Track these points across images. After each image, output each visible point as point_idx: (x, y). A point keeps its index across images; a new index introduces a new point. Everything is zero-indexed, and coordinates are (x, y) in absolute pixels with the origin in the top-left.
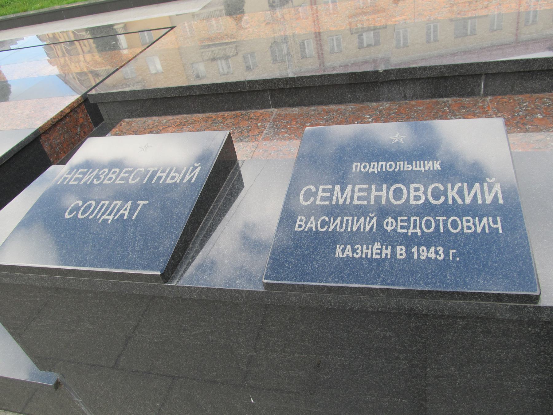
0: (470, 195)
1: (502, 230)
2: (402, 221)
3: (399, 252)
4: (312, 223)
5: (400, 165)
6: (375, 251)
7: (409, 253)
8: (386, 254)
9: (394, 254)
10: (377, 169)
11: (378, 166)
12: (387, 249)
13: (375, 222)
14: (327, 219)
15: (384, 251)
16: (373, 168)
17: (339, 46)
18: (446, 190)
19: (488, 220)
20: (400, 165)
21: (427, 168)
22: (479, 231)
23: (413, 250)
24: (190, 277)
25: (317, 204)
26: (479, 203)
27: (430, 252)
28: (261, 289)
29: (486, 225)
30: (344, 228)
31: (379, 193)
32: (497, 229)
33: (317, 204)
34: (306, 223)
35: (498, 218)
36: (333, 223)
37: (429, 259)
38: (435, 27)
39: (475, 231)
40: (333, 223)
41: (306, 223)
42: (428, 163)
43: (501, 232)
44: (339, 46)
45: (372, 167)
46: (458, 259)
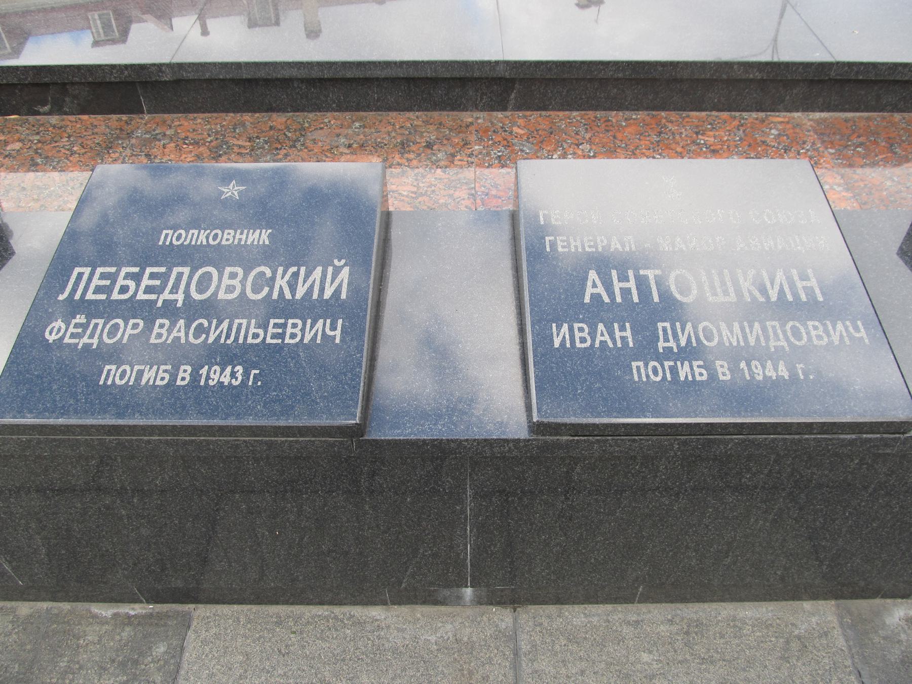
14: (206, 324)
18: (273, 279)
19: (324, 325)
26: (287, 297)
27: (780, 369)
28: (523, 434)
30: (232, 338)
32: (862, 338)
33: (138, 298)
35: (340, 322)
37: (221, 384)
39: (831, 343)
40: (222, 332)
41: (170, 331)
46: (259, 383)
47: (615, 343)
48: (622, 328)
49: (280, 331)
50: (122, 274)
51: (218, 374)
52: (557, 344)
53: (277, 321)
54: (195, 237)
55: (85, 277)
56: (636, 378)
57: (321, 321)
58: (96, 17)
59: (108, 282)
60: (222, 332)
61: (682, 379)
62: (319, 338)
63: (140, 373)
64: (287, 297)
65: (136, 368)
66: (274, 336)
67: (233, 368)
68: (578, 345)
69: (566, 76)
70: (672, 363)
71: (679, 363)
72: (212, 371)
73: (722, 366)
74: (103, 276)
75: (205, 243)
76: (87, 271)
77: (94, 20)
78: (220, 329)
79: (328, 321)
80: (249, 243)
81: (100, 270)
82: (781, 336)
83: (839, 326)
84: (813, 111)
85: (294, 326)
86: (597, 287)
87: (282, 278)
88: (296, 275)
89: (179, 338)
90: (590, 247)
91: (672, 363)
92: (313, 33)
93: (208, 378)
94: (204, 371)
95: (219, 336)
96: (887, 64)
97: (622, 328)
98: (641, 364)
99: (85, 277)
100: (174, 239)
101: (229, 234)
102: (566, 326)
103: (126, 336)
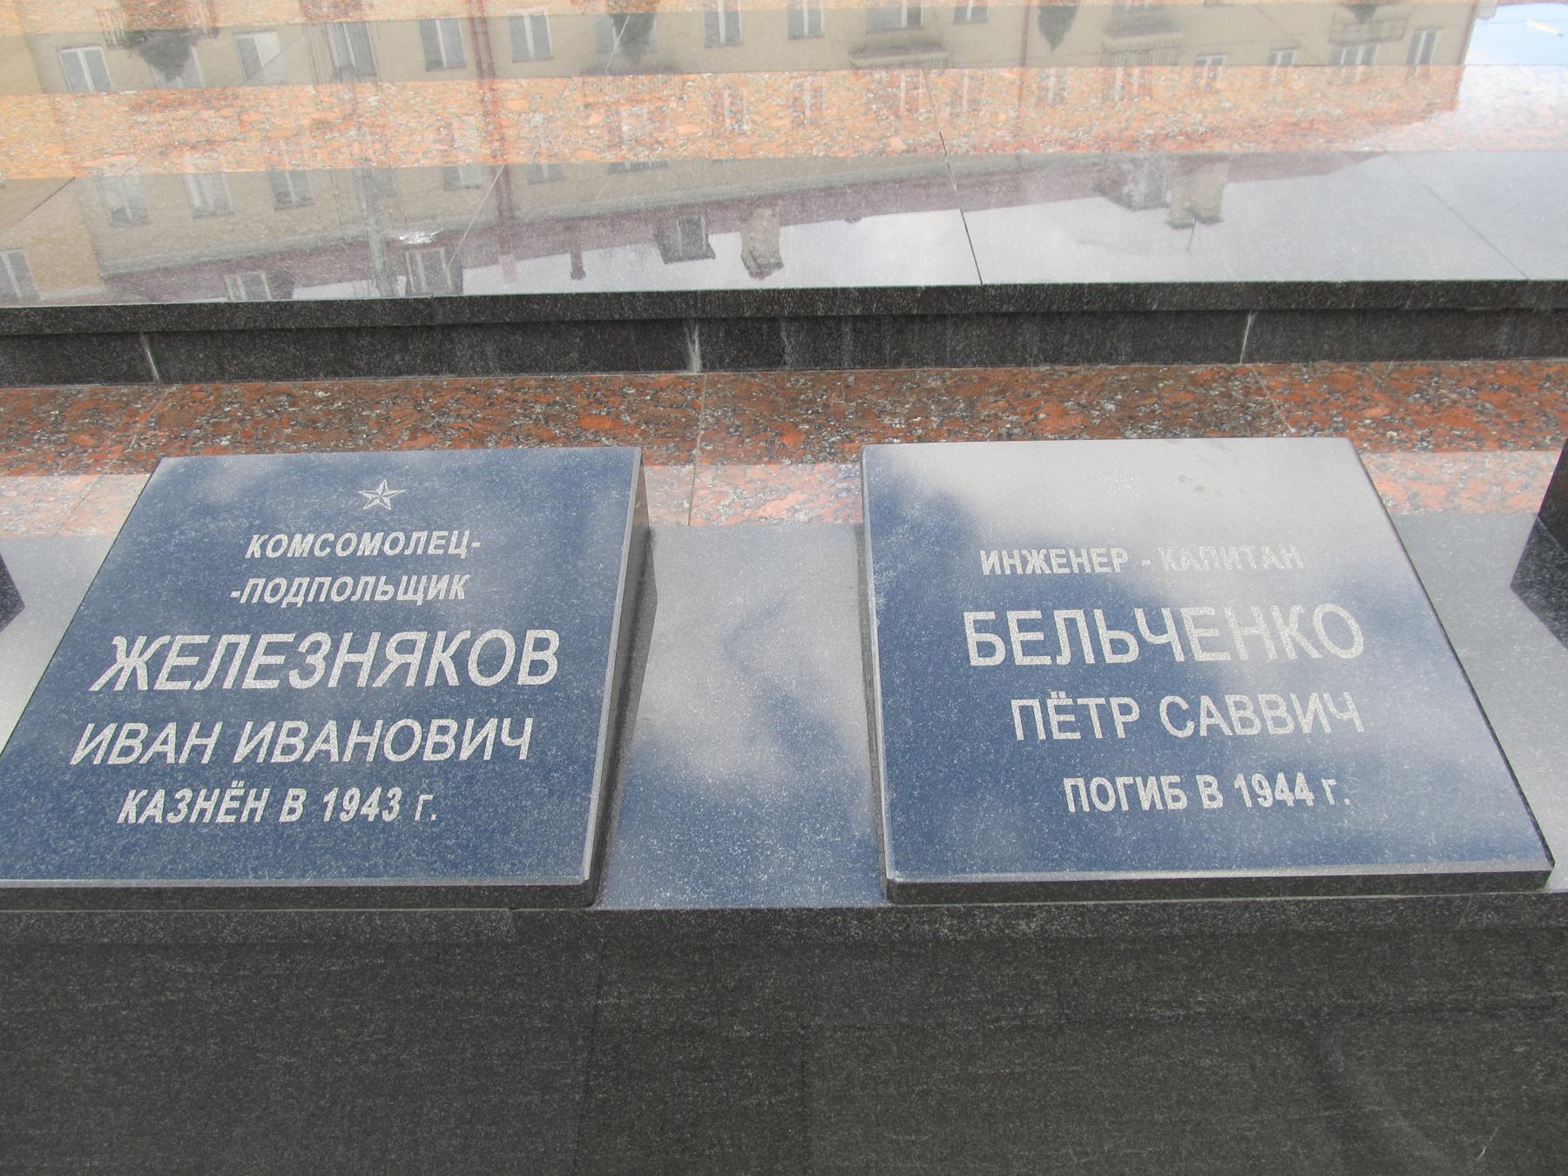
2: (1058, 556)
3: (289, 803)
4: (1210, 715)
5: (300, 585)
6: (216, 807)
8: (253, 811)
9: (1195, 798)
10: (306, 595)
11: (308, 590)
12: (258, 798)
13: (243, 741)
15: (250, 804)
16: (296, 594)
17: (817, 107)
20: (300, 585)
25: (244, 686)
26: (451, 683)
33: (244, 686)
37: (1279, 804)
38: (1431, 38)
40: (250, 739)
41: (309, 742)
44: (817, 107)
45: (294, 589)
50: (176, 648)
51: (357, 796)
54: (370, 588)
55: (241, 652)
56: (1072, 808)
57: (493, 722)
59: (193, 661)
60: (250, 739)
61: (1146, 806)
63: (171, 805)
64: (451, 683)
67: (385, 791)
70: (1129, 780)
71: (1139, 780)
72: (347, 798)
73: (1208, 785)
74: (272, 649)
75: (257, 555)
76: (244, 640)
79: (507, 722)
81: (266, 639)
83: (1314, 703)
87: (444, 649)
89: (163, 755)
91: (1129, 780)
92: (578, 272)
93: (338, 808)
94: (330, 798)
95: (256, 751)
99: (241, 652)
100: (268, 593)
103: (377, 731)
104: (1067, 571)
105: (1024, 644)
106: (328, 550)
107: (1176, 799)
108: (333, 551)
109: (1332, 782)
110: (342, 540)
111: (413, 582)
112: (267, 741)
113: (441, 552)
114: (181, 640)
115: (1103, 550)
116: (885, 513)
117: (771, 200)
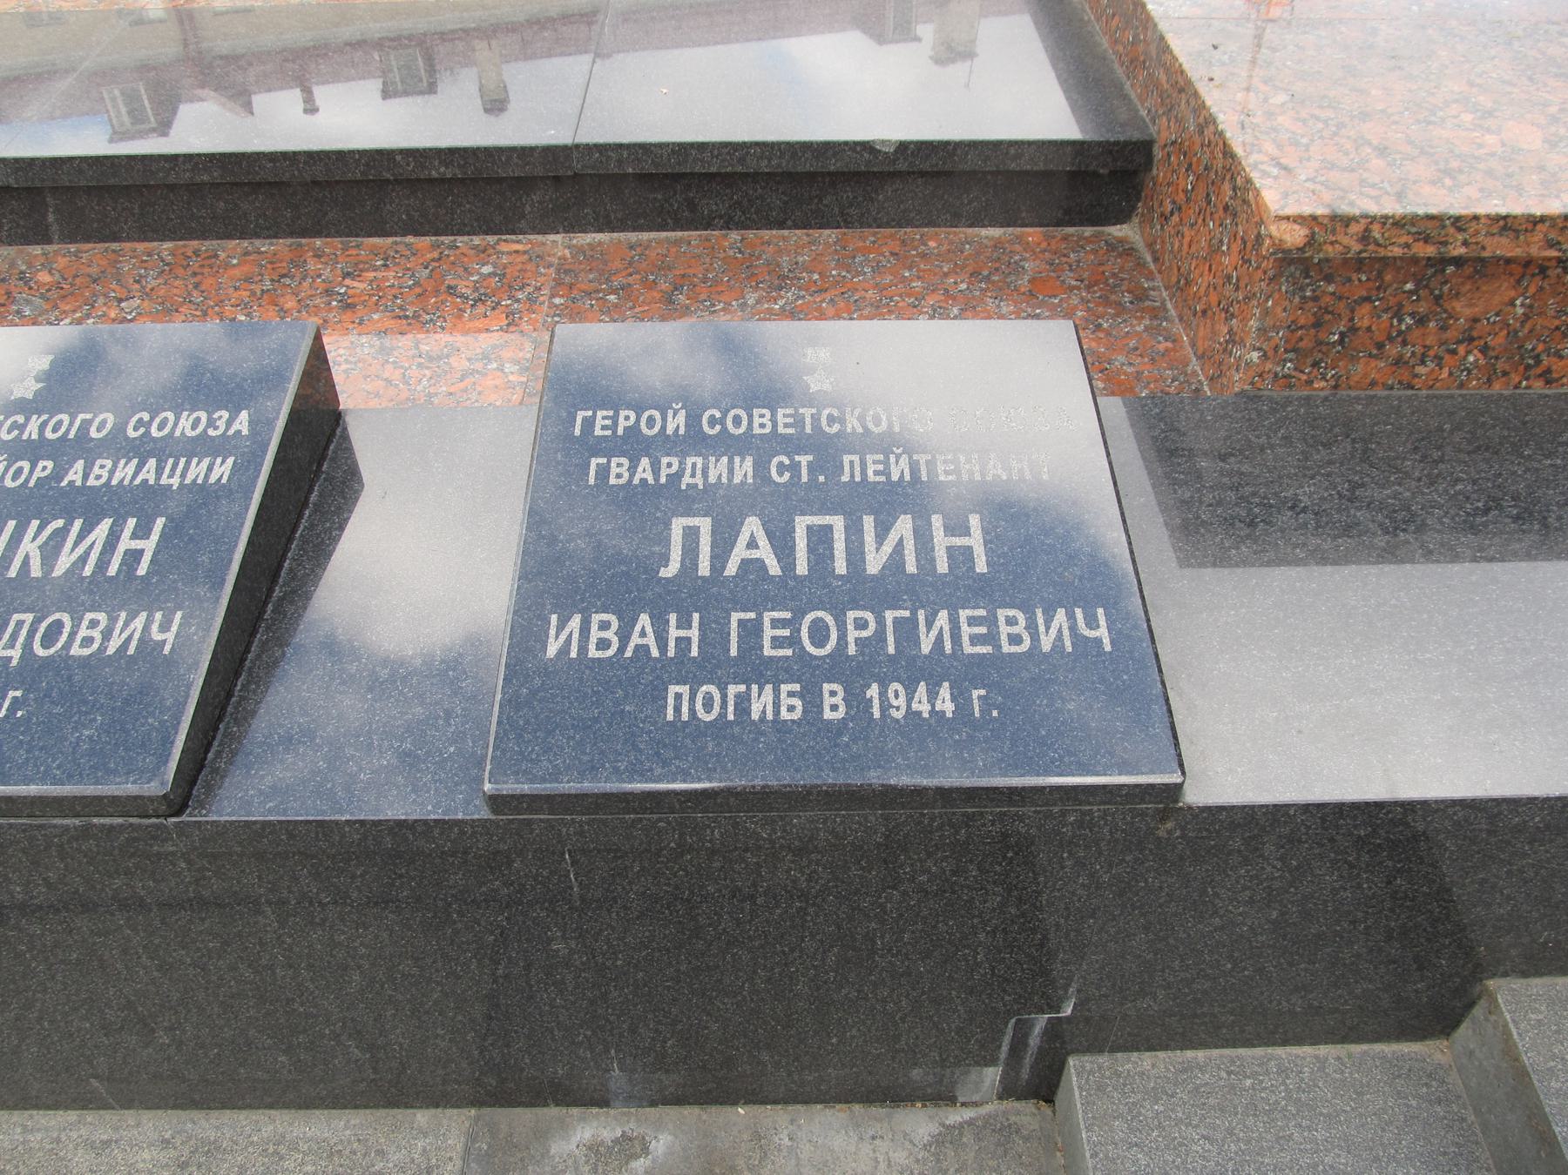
0: (748, 535)
1: (1112, 642)
2: (972, 621)
7: (856, 699)
16: (693, 475)
21: (712, 479)
22: (1046, 644)
23: (869, 694)
24: (254, 792)
26: (772, 572)
27: (916, 699)
28: (485, 813)
29: (1066, 633)
31: (683, 633)
32: (1098, 641)
34: (624, 638)
36: (87, 553)
40: (87, 553)
41: (624, 638)
42: (742, 461)
43: (1108, 648)
47: (663, 647)
48: (684, 623)
49: (786, 632)
52: (926, 648)
53: (776, 615)
56: (670, 716)
58: (117, 92)
61: (755, 716)
62: (134, 644)
64: (772, 572)
65: (733, 690)
66: (975, 640)
68: (593, 653)
69: (112, 181)
71: (755, 687)
73: (833, 693)
77: (113, 99)
78: (124, 636)
80: (212, 480)
82: (699, 472)
84: (584, 232)
85: (93, 624)
86: (757, 547)
87: (34, 539)
88: (61, 534)
90: (947, 473)
94: (873, 691)
96: (667, 145)
97: (684, 623)
98: (684, 690)
101: (762, 416)
102: (943, 616)
104: (883, 479)
105: (774, 639)
106: (718, 427)
107: (791, 709)
108: (148, 433)
109: (983, 692)
110: (158, 420)
111: (181, 465)
112: (576, 636)
113: (609, 433)
114: (768, 617)
115: (881, 457)
116: (569, 392)
117: (490, 31)
